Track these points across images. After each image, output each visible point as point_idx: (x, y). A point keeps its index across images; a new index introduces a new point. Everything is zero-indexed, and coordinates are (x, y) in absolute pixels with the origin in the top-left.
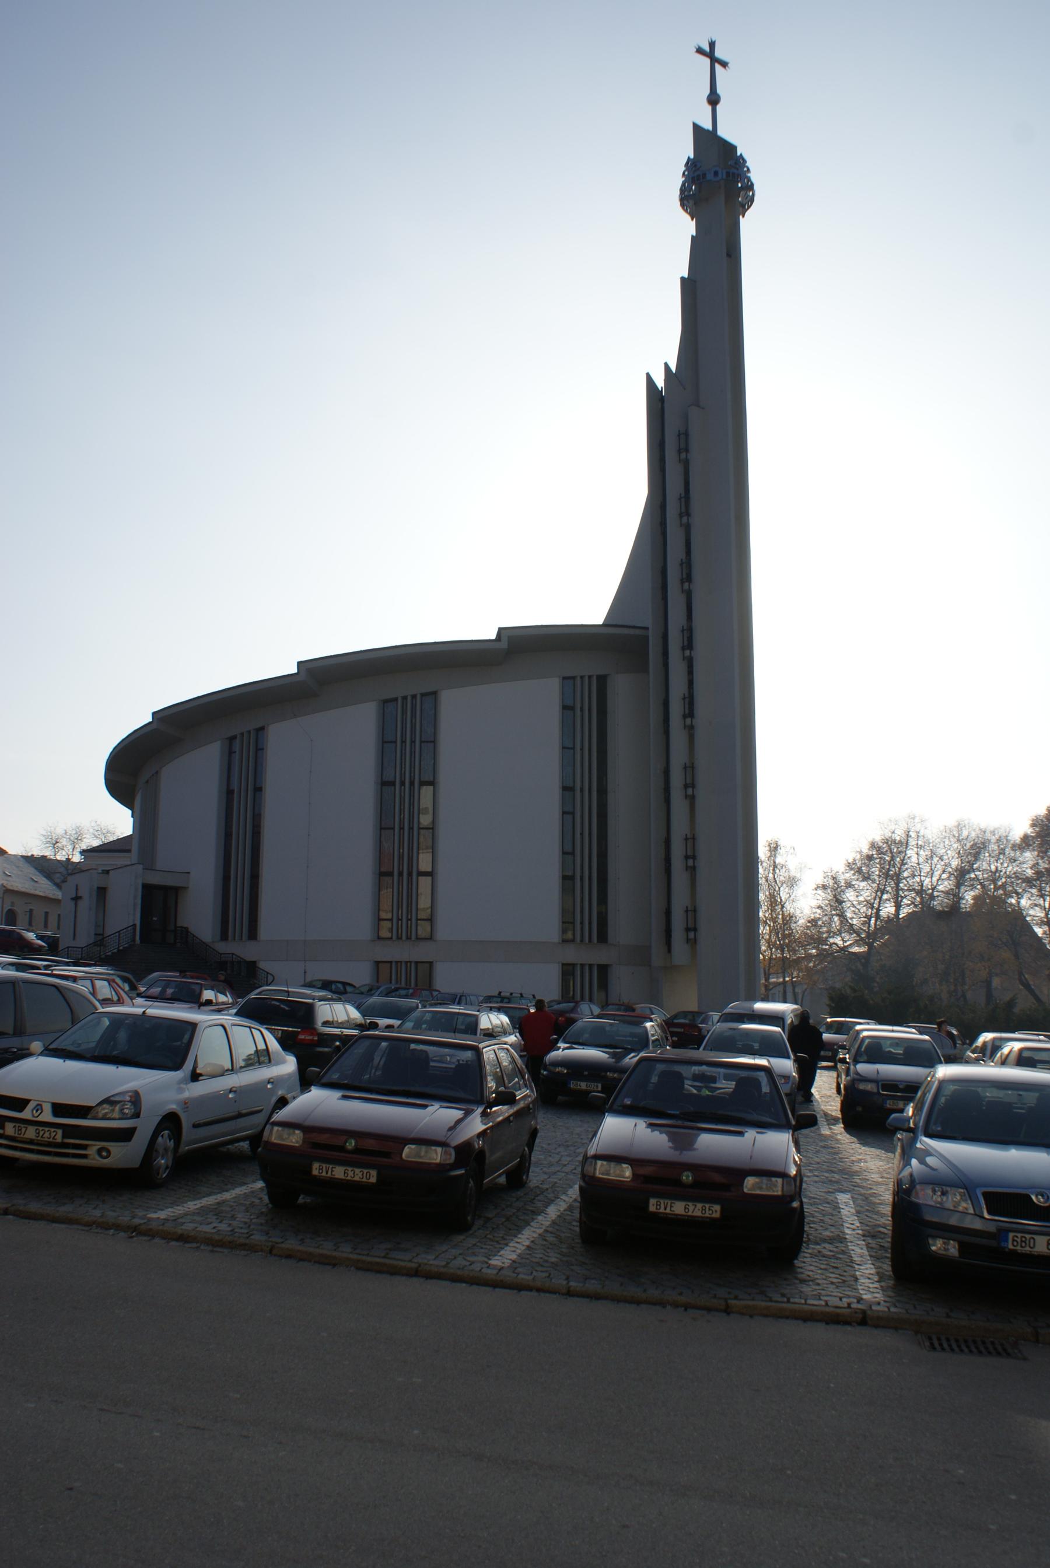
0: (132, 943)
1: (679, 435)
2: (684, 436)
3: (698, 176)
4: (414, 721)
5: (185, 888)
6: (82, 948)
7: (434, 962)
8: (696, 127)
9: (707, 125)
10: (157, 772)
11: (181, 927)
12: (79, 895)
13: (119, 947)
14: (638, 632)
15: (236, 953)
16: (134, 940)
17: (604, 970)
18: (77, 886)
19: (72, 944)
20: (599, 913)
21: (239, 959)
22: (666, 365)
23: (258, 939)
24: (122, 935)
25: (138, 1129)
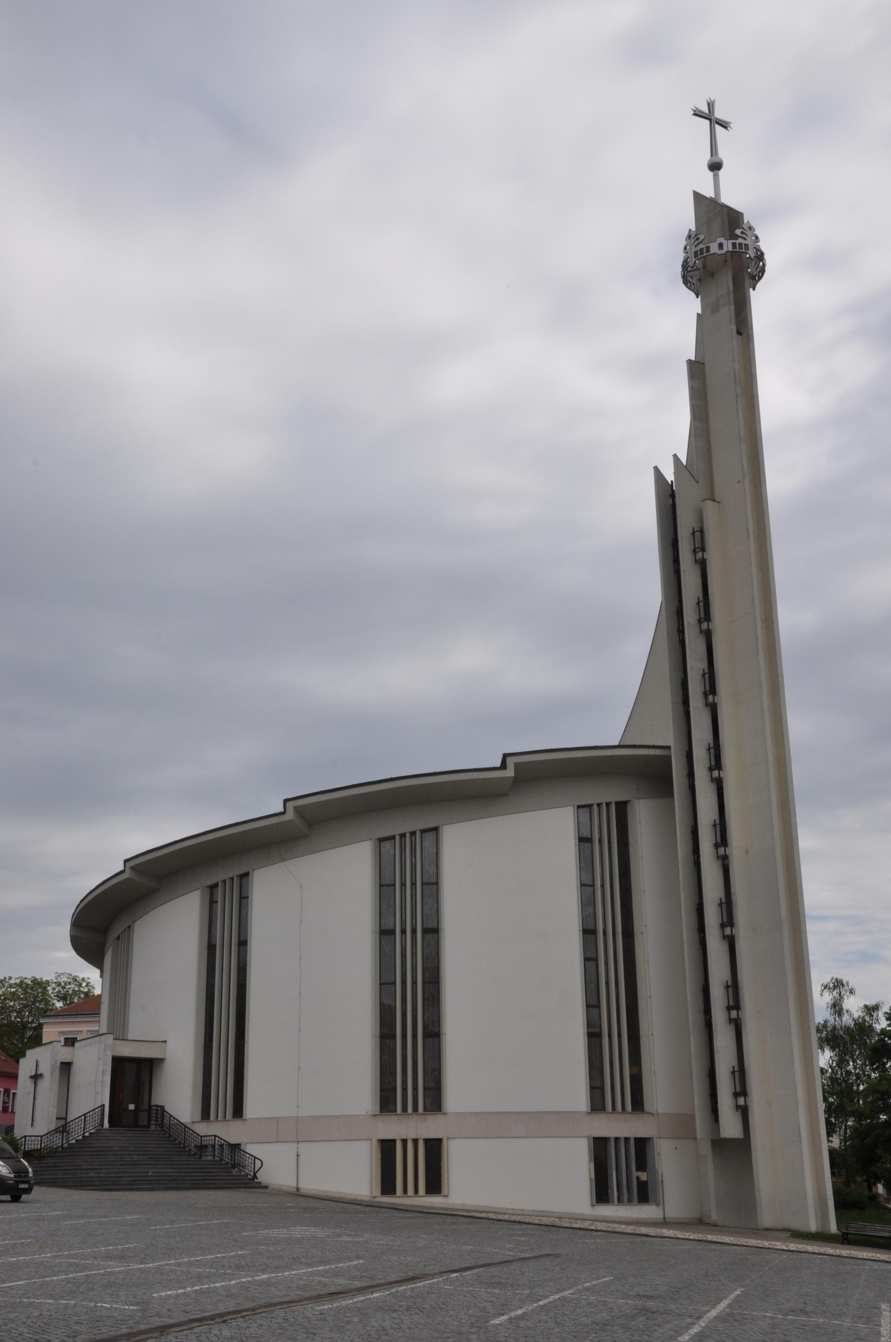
0: (100, 1127)
1: (693, 534)
2: (699, 536)
3: (702, 250)
4: (414, 859)
5: (161, 1060)
6: (41, 1137)
7: (445, 1141)
8: (697, 196)
9: (709, 193)
10: (129, 927)
11: (157, 1106)
12: (39, 1072)
13: (84, 1133)
14: (658, 752)
15: (218, 1135)
16: (102, 1125)
17: (642, 1145)
18: (37, 1061)
19: (29, 1132)
20: (632, 1076)
21: (223, 1142)
22: (675, 457)
23: (244, 1118)
24: (88, 1119)
25: (695, 190)
